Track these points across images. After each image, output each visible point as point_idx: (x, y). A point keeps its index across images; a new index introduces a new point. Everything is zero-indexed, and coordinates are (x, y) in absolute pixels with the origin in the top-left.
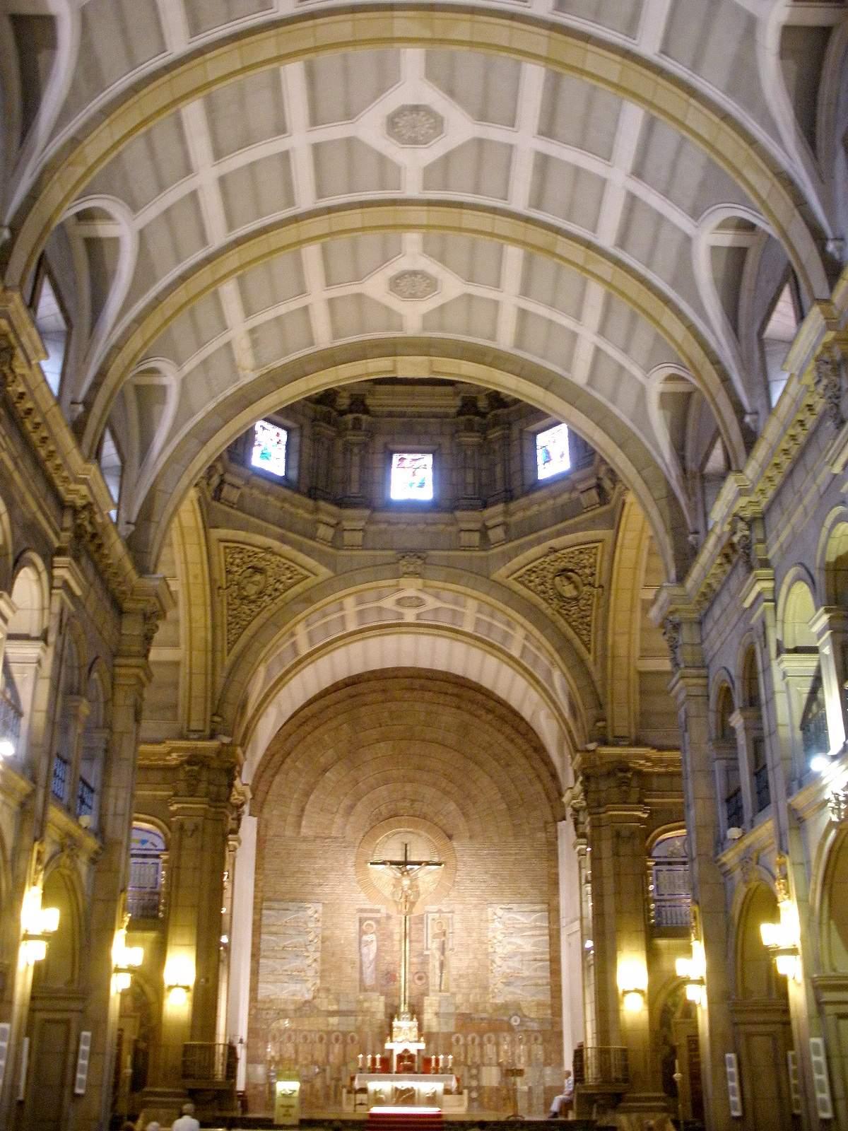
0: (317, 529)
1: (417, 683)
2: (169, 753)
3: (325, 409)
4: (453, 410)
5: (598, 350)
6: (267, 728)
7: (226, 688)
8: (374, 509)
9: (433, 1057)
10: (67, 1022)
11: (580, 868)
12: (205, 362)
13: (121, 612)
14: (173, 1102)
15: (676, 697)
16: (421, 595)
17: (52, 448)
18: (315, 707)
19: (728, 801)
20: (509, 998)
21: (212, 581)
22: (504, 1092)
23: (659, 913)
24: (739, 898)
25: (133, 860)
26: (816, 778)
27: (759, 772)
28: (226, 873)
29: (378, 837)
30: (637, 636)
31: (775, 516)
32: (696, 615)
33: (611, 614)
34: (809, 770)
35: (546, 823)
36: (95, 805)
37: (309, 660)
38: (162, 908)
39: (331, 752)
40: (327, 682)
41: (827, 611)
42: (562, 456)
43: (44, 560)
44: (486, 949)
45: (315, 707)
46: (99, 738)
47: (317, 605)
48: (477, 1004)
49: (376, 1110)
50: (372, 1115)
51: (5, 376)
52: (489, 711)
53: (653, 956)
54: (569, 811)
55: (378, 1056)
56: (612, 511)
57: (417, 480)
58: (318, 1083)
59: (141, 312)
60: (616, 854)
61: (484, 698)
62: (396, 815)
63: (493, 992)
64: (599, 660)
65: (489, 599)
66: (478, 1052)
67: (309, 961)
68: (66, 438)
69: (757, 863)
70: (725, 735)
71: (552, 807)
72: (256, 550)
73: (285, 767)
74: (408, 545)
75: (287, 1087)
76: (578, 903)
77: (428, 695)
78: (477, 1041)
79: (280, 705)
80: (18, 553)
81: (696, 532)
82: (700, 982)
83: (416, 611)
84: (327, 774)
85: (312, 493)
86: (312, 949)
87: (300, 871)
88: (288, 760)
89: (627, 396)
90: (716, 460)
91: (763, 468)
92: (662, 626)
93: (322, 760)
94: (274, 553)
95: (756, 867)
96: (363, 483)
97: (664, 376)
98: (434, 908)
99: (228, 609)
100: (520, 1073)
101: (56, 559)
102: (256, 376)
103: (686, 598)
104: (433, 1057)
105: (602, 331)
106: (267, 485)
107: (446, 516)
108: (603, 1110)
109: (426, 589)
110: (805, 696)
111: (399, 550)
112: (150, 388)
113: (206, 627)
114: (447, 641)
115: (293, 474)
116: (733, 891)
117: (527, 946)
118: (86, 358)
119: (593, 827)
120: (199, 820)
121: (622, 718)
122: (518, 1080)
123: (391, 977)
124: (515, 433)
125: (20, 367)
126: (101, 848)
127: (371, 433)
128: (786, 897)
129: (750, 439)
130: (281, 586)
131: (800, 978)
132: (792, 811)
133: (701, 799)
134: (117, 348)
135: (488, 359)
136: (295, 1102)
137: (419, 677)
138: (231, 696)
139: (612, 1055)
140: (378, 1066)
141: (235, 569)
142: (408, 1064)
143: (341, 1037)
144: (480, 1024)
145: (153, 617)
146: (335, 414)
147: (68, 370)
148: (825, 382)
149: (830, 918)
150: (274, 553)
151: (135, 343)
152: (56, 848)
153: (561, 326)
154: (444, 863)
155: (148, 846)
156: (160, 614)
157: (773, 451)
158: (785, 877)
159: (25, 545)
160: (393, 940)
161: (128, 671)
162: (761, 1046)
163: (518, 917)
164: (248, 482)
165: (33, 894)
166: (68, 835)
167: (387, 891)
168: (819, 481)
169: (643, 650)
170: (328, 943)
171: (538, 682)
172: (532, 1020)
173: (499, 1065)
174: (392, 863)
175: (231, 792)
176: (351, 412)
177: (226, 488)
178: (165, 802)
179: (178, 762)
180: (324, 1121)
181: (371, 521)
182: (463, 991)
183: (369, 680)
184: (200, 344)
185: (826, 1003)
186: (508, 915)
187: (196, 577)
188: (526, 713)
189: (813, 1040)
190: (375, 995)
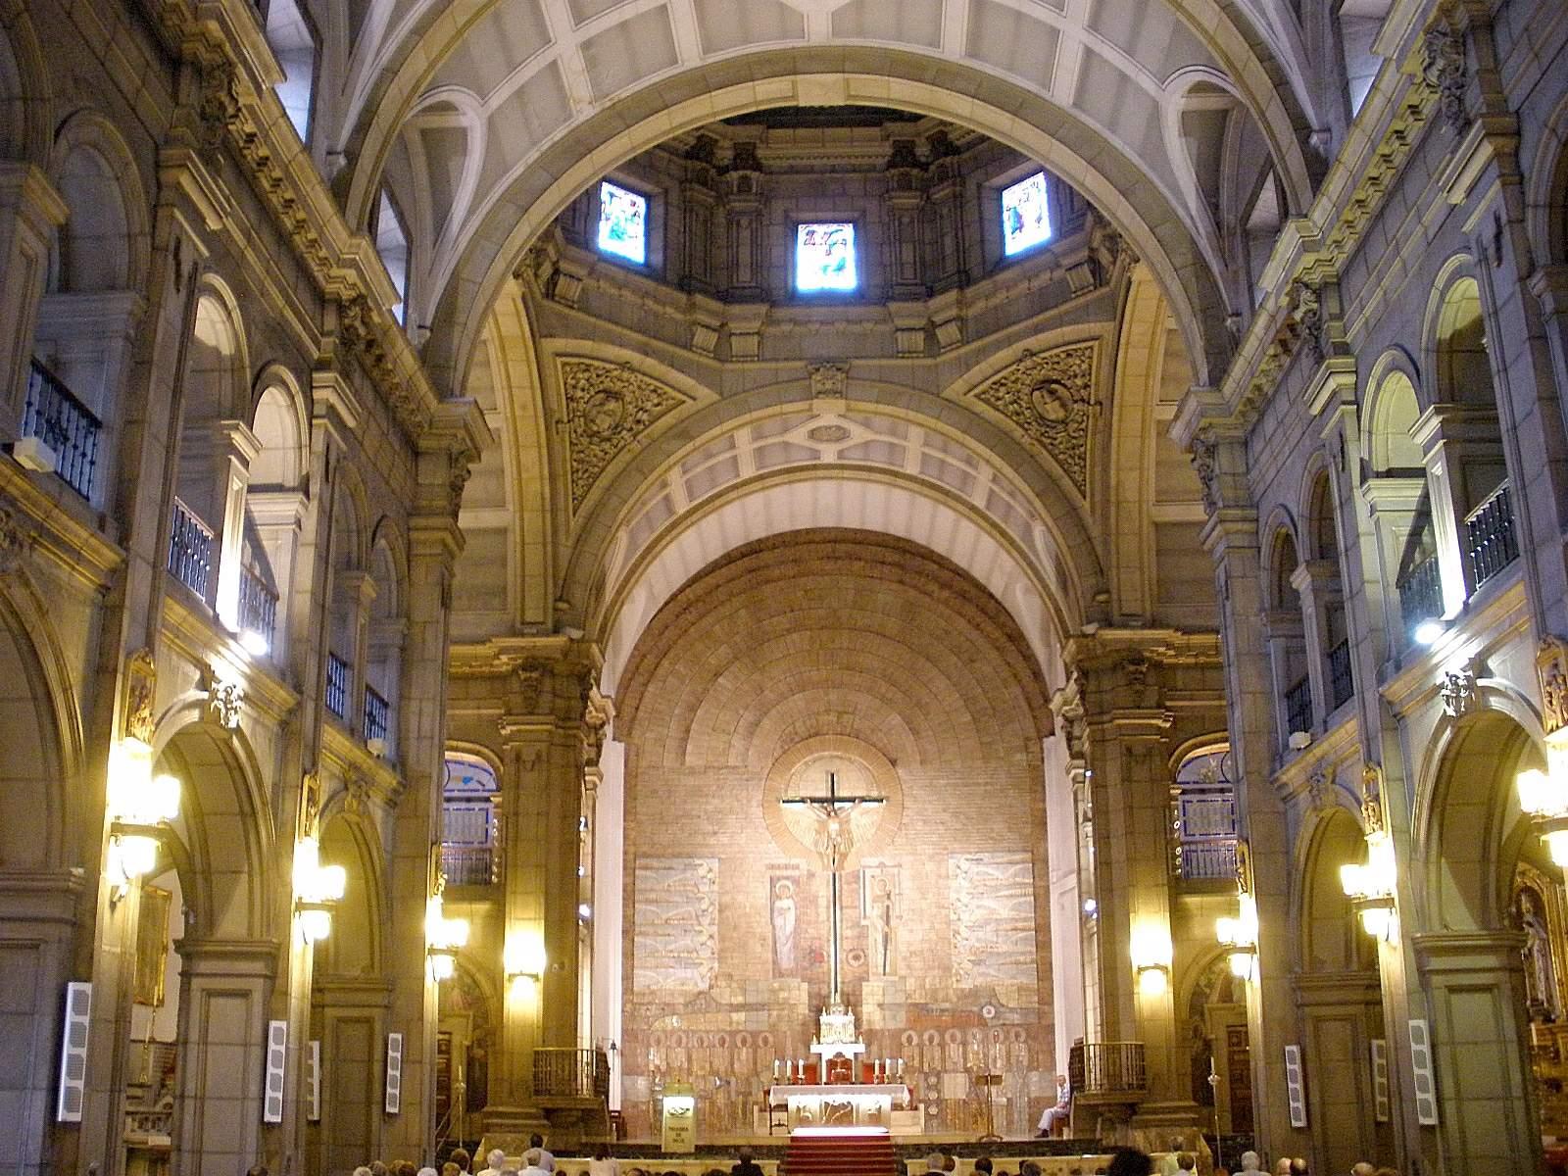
0: (693, 335)
1: (842, 548)
2: (497, 656)
3: (699, 165)
4: (881, 162)
5: (1089, 52)
6: (634, 618)
7: (573, 563)
8: (773, 304)
9: (877, 1062)
10: (368, 1021)
11: (1076, 801)
12: (520, 93)
13: (416, 454)
14: (526, 1126)
15: (1211, 552)
16: (844, 424)
17: (301, 215)
18: (699, 588)
19: (1289, 695)
20: (979, 981)
21: (547, 412)
22: (975, 1105)
23: (1187, 860)
24: (1306, 833)
25: (453, 806)
26: (1421, 654)
27: (1337, 653)
28: (583, 819)
29: (794, 764)
30: (1151, 474)
31: (1356, 280)
32: (1239, 433)
33: (1114, 442)
34: (1409, 642)
35: (1027, 739)
36: (390, 724)
37: (689, 521)
38: (495, 869)
39: (723, 650)
40: (715, 553)
41: (1438, 412)
42: (1039, 220)
43: (299, 379)
44: (947, 916)
45: (699, 588)
46: (393, 631)
47: (698, 442)
48: (935, 991)
49: (800, 1132)
50: (793, 1139)
51: (222, 106)
52: (943, 586)
53: (1179, 919)
54: (1059, 721)
55: (801, 1063)
56: (1113, 296)
57: (833, 261)
58: (721, 1099)
59: (421, 20)
60: (1127, 779)
61: (936, 567)
62: (817, 734)
63: (958, 973)
64: (1098, 511)
65: (940, 426)
66: (937, 1054)
67: (703, 938)
68: (322, 202)
69: (1333, 782)
70: (1285, 601)
71: (1034, 717)
72: (608, 366)
73: (660, 671)
74: (824, 352)
75: (678, 1104)
76: (1075, 850)
77: (857, 565)
78: (936, 1041)
79: (651, 587)
80: (259, 364)
81: (1237, 314)
82: (1251, 950)
83: (836, 447)
84: (721, 680)
85: (685, 284)
86: (705, 921)
87: (687, 815)
88: (666, 663)
89: (1134, 119)
90: (1267, 203)
91: (1339, 208)
92: (1190, 449)
93: (713, 661)
94: (632, 370)
95: (1331, 787)
96: (756, 267)
97: (1187, 88)
98: (874, 861)
99: (572, 452)
100: (996, 1080)
101: (315, 375)
102: (598, 109)
103: (1225, 409)
104: (877, 1062)
105: (1094, 25)
106: (621, 275)
107: (876, 311)
108: (1110, 1124)
109: (850, 414)
110: (1404, 539)
111: (811, 361)
112: (442, 131)
113: (542, 478)
114: (881, 488)
115: (657, 259)
116: (1297, 823)
117: (1004, 910)
118: (345, 88)
119: (1093, 742)
120: (543, 746)
121: (1132, 589)
122: (994, 1089)
123: (816, 956)
124: (971, 186)
125: (245, 95)
126: (399, 783)
127: (766, 197)
128: (1376, 827)
129: (1318, 169)
130: (645, 417)
131: (1396, 939)
132: (1385, 704)
133: (1251, 696)
134: (390, 72)
135: (929, 75)
136: (689, 1123)
137: (844, 541)
138: (580, 575)
139: (1124, 1054)
140: (801, 1075)
141: (579, 394)
142: (842, 1072)
143: (749, 1040)
144: (942, 1018)
145: (461, 459)
146: (713, 172)
147: (320, 105)
148: (1440, 63)
149: (1440, 854)
150: (632, 370)
151: (418, 63)
152: (335, 785)
153: (1037, 22)
154: (887, 798)
155: (473, 785)
156: (475, 454)
157: (1354, 182)
158: (1377, 798)
159: (268, 355)
160: (817, 906)
161: (428, 536)
162: (1335, 1037)
163: (991, 871)
164: (592, 272)
165: (306, 849)
166: (354, 766)
167: (808, 840)
168: (1427, 218)
169: (1158, 492)
170: (728, 913)
171: (1012, 542)
172: (1012, 1010)
173: (967, 1070)
174: (813, 800)
175: (586, 707)
176: (736, 169)
177: (562, 280)
178: (495, 723)
179: (510, 668)
180: (727, 1147)
181: (770, 321)
182: (915, 974)
183: (775, 547)
184: (512, 66)
185: (1431, 972)
186: (975, 868)
187: (524, 407)
188: (996, 587)
189: (1412, 1023)
190: (795, 982)
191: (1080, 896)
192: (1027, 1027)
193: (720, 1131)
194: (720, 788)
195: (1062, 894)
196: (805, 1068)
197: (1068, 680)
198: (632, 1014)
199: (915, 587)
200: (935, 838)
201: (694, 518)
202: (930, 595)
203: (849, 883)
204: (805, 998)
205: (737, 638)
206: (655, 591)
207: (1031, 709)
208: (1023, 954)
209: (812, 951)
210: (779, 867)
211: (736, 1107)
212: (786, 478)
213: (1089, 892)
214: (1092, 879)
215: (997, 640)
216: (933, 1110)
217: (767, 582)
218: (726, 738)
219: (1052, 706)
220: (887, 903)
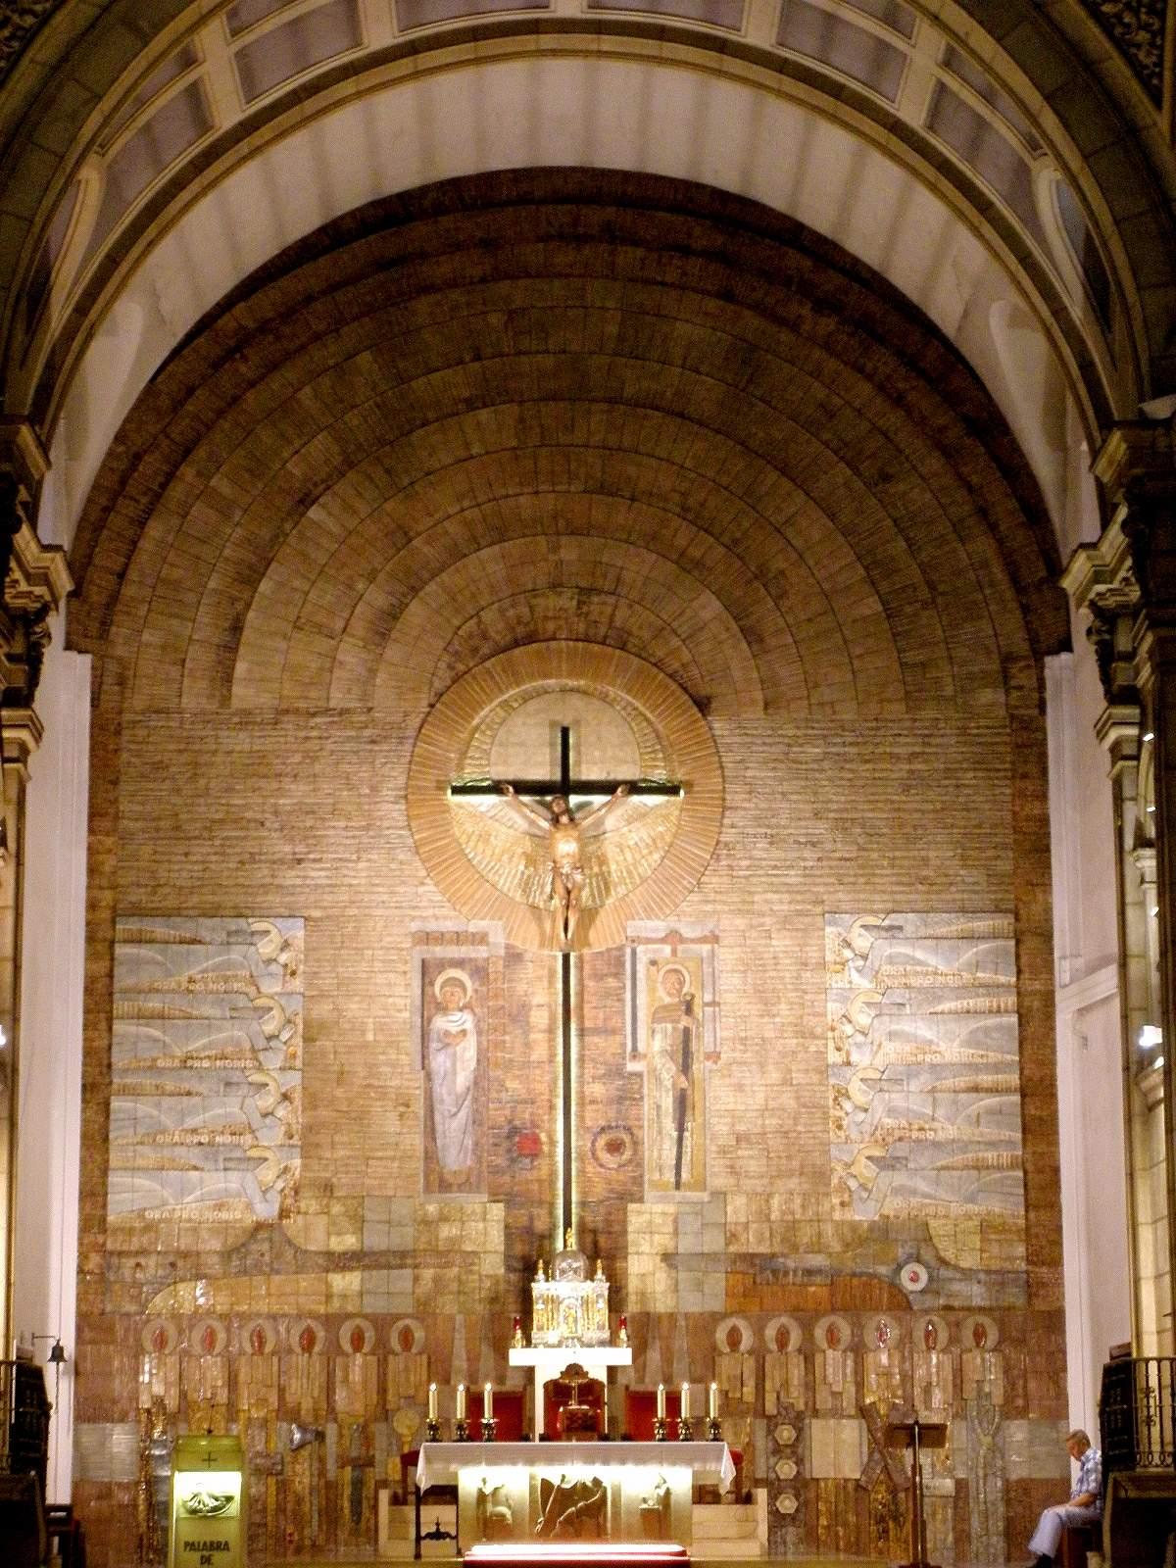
1: (595, 217)
18: (267, 301)
20: (893, 1206)
22: (881, 1495)
29: (477, 706)
35: (1007, 659)
37: (244, 147)
40: (304, 221)
44: (821, 1054)
45: (267, 301)
48: (793, 1226)
52: (822, 306)
54: (1082, 619)
55: (488, 1388)
58: (302, 1476)
62: (531, 638)
63: (843, 1187)
66: (797, 1373)
67: (268, 1101)
71: (1026, 609)
73: (176, 492)
79: (155, 295)
84: (314, 513)
86: (274, 1061)
88: (188, 472)
93: (295, 468)
98: (657, 927)
100: (933, 1435)
122: (926, 1457)
123: (523, 1143)
136: (231, 1532)
140: (488, 1417)
142: (582, 1411)
143: (370, 1335)
144: (803, 1290)
154: (689, 785)
160: (527, 1028)
163: (919, 955)
167: (508, 876)
170: (325, 1043)
171: (984, 207)
172: (967, 1274)
174: (522, 787)
182: (748, 1184)
188: (945, 309)
191: (1125, 1017)
192: (1001, 1314)
193: (298, 1551)
194: (311, 757)
195: (1082, 1012)
196: (499, 1400)
197: (1105, 523)
198: (102, 1277)
199: (757, 308)
200: (794, 877)
201: (256, 139)
202: (794, 326)
203: (599, 977)
204: (496, 1239)
205: (353, 419)
206: (166, 306)
207: (1019, 588)
208: (992, 1144)
209: (514, 1131)
210: (440, 938)
211: (339, 1496)
212: (464, 51)
213: (1144, 1009)
214: (1155, 978)
215: (943, 429)
216: (787, 1505)
217: (428, 289)
218: (323, 644)
219: (1069, 583)
220: (685, 1021)
